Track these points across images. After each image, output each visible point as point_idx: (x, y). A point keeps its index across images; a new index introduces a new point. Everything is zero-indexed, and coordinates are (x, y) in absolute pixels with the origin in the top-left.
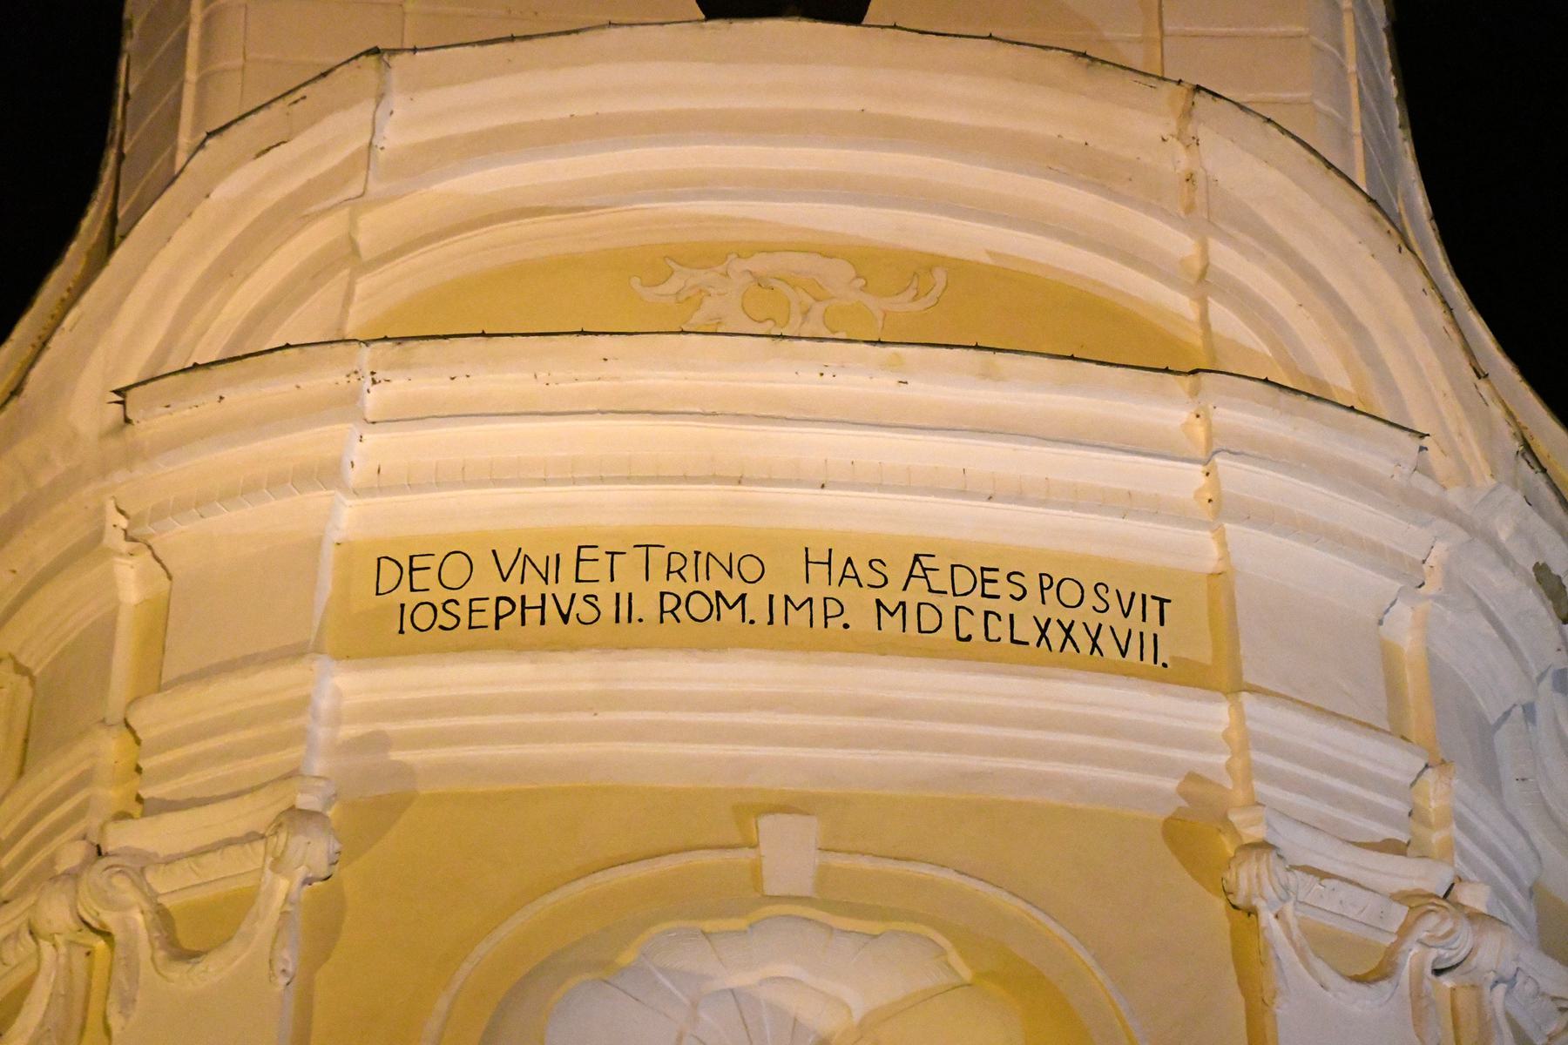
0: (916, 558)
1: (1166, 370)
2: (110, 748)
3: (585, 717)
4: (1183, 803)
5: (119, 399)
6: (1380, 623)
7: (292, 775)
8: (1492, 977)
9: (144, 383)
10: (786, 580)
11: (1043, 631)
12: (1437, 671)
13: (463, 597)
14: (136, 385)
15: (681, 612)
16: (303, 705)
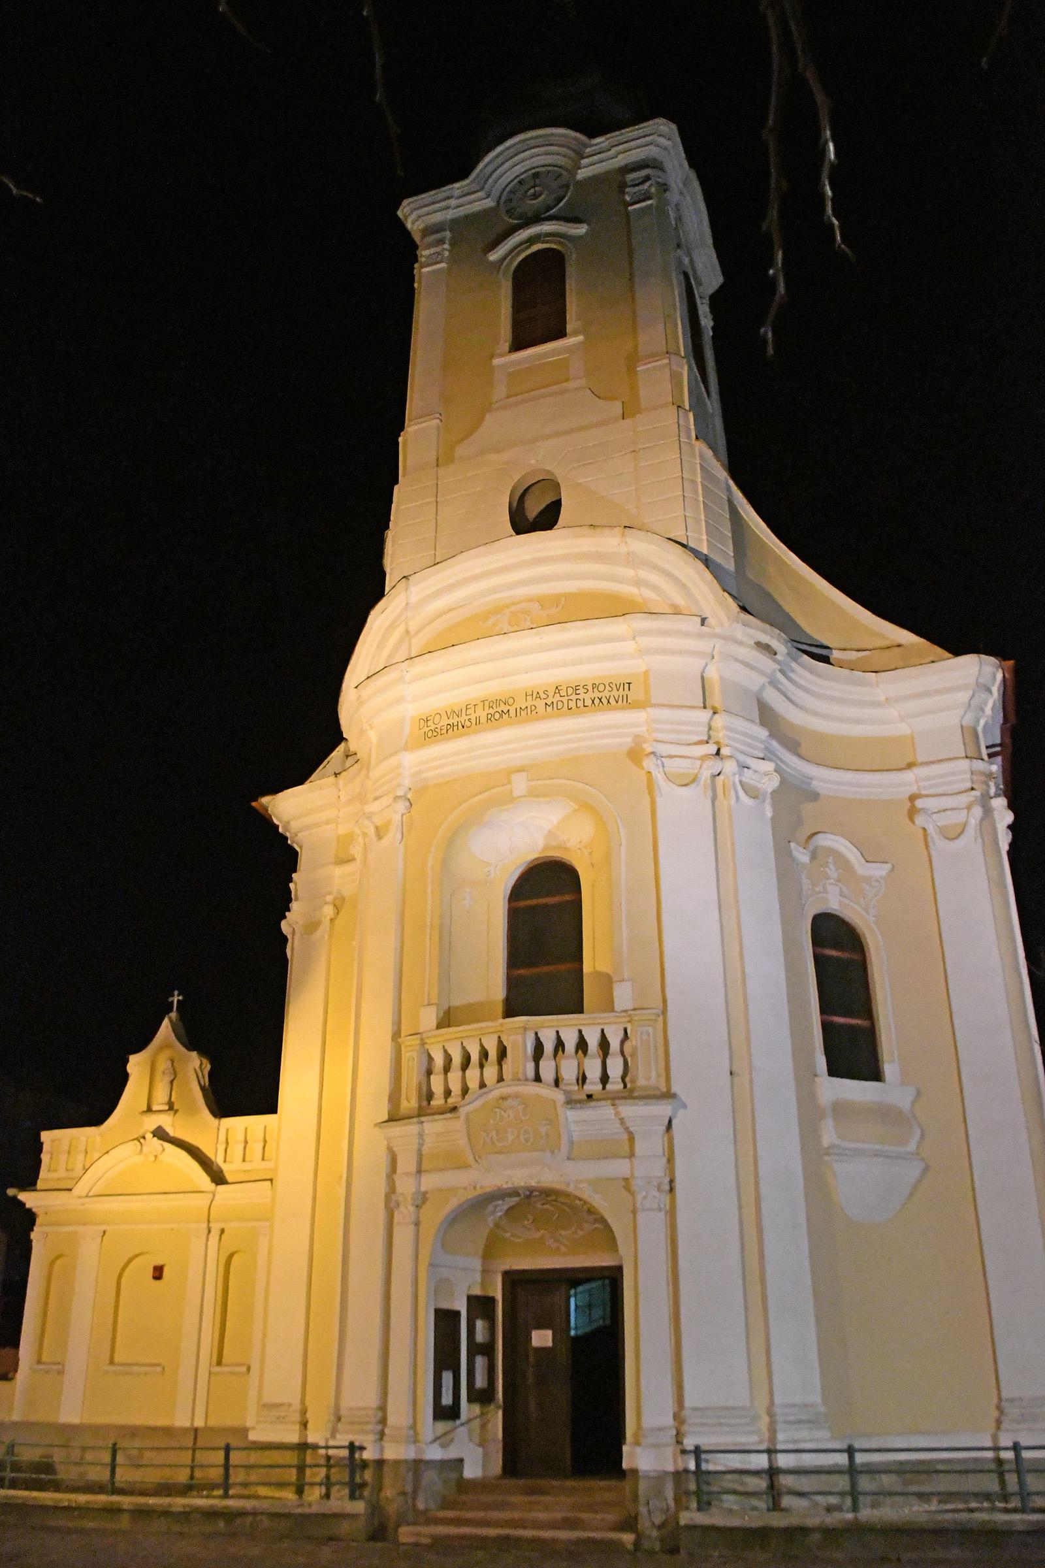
0: (557, 688)
11: (593, 701)
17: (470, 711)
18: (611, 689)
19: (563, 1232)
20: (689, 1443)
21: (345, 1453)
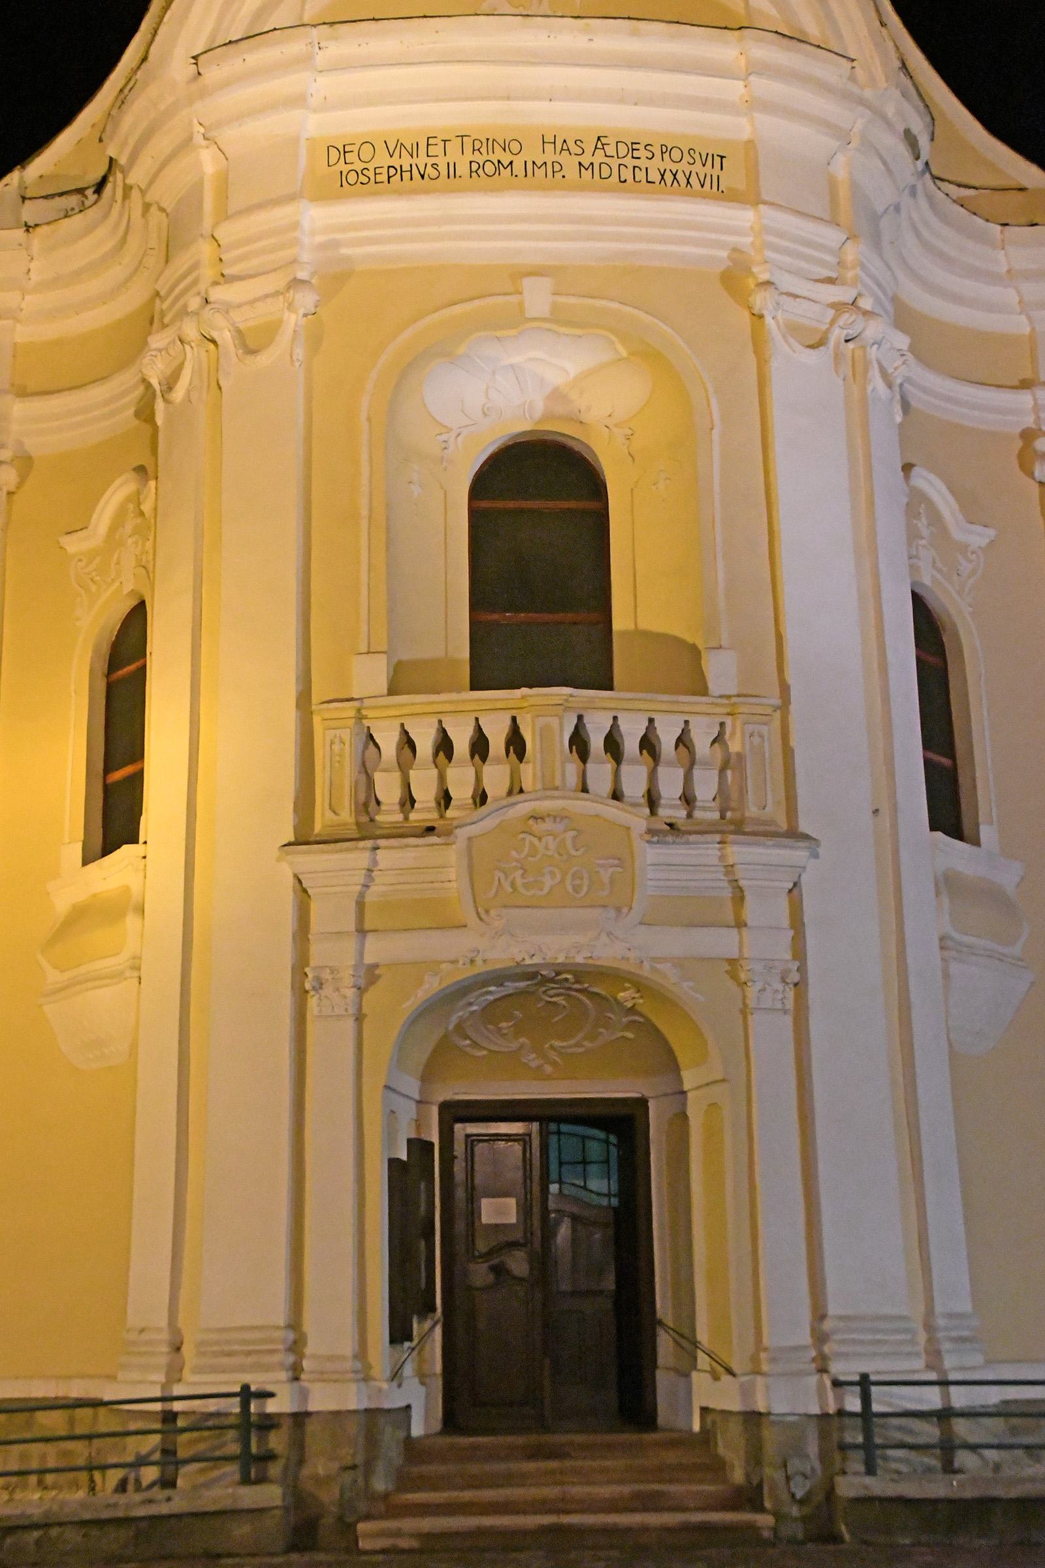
0: (599, 139)
1: (726, 28)
2: (205, 250)
3: (435, 229)
4: (731, 264)
5: (195, 61)
6: (829, 164)
7: (294, 261)
8: (872, 341)
9: (205, 52)
10: (533, 153)
11: (663, 176)
12: (854, 186)
13: (371, 166)
14: (202, 53)
15: (480, 171)
16: (296, 226)
17: (436, 150)
18: (692, 161)
19: (557, 1043)
20: (845, 1369)
21: (233, 1406)
